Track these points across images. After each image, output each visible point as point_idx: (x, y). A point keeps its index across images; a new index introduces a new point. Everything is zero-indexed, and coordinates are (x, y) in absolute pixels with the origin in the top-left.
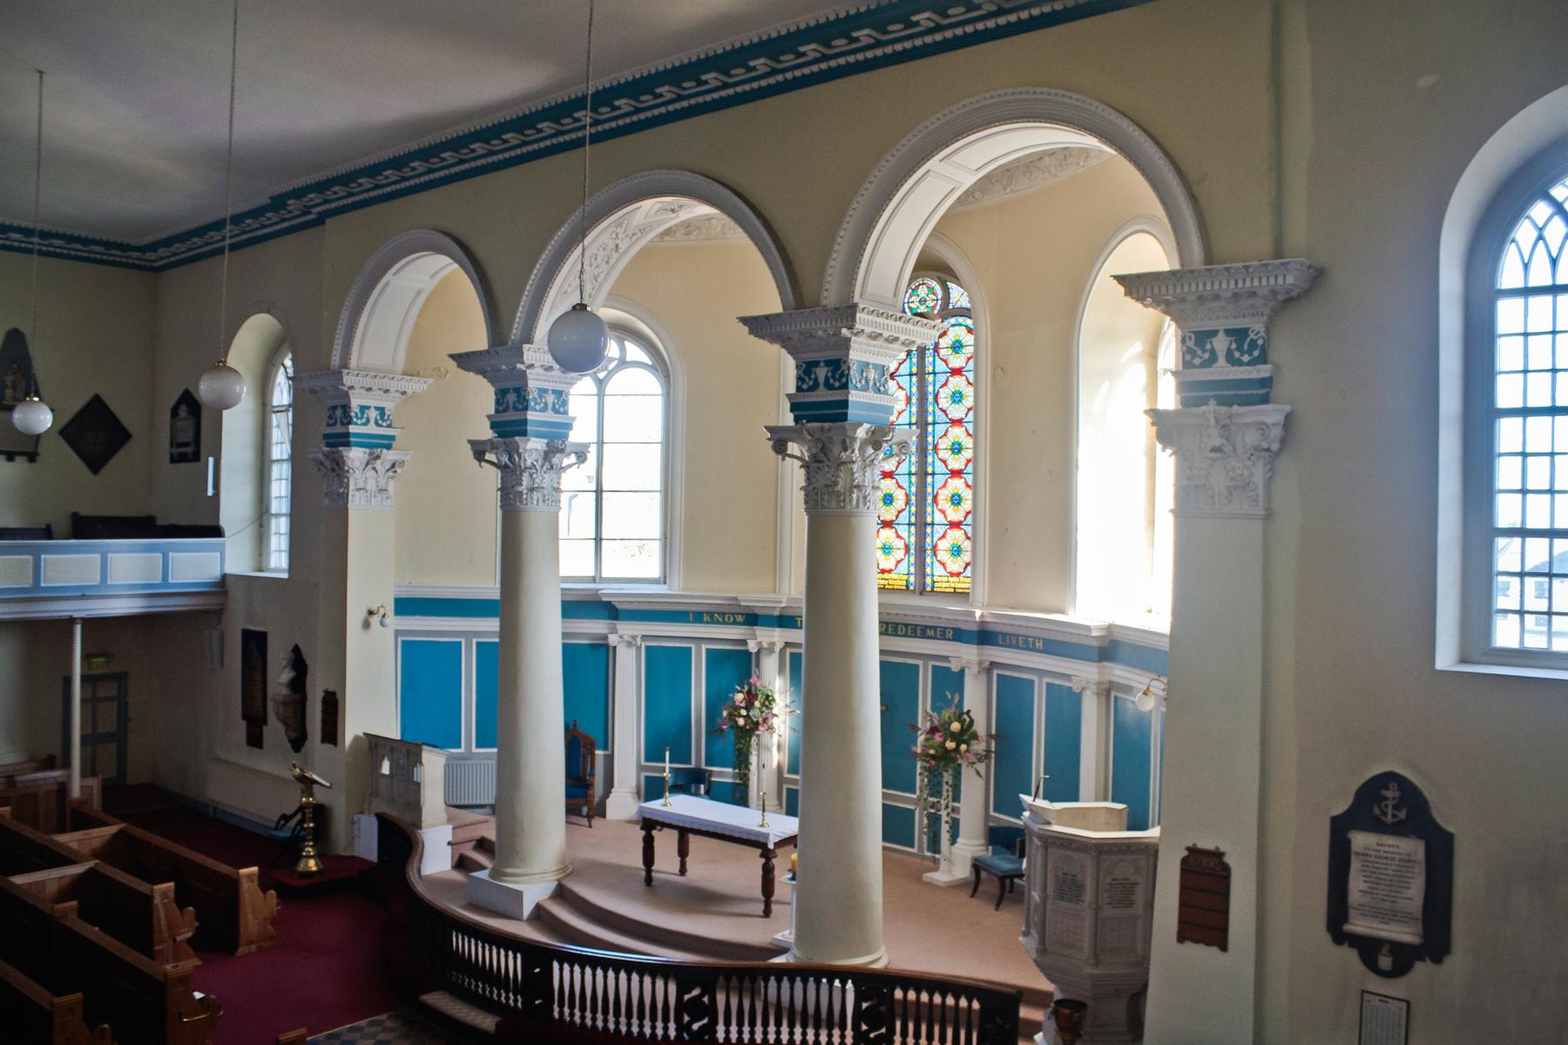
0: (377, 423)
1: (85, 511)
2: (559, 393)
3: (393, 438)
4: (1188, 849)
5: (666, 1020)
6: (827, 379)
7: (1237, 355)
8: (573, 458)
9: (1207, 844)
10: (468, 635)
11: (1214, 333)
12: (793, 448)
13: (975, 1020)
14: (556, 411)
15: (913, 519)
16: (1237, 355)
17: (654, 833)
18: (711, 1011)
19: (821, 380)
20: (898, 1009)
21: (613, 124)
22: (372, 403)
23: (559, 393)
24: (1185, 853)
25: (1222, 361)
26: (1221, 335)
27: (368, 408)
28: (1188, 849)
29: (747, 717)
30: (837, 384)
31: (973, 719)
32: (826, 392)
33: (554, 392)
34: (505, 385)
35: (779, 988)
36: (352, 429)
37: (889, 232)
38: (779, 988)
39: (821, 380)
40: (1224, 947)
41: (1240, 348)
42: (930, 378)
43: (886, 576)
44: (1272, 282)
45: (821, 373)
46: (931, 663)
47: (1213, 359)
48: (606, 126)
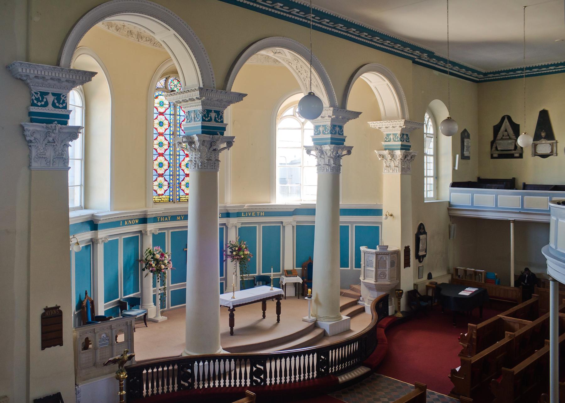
0: (54, 105)
1: (483, 177)
2: (218, 113)
3: (410, 146)
4: (45, 309)
5: (313, 371)
6: (393, 139)
7: (57, 105)
8: (225, 145)
9: (51, 305)
10: (352, 223)
11: (47, 94)
12: (313, 152)
13: (176, 373)
14: (339, 134)
15: (171, 173)
16: (57, 105)
17: (281, 301)
18: (265, 372)
19: (213, 119)
20: (144, 378)
21: (279, 13)
22: (50, 90)
23: (218, 113)
24: (44, 311)
25: (50, 105)
26: (50, 95)
27: (47, 94)
28: (45, 309)
29: (243, 255)
30: (219, 121)
31: (258, 252)
32: (215, 123)
33: (215, 112)
34: (209, 108)
35: (230, 364)
36: (400, 143)
37: (389, 91)
38: (230, 364)
39: (213, 119)
40: (42, 349)
41: (59, 102)
42: (178, 117)
43: (160, 197)
44: (36, 72)
45: (213, 115)
46: (171, 231)
47: (46, 104)
48: (276, 12)
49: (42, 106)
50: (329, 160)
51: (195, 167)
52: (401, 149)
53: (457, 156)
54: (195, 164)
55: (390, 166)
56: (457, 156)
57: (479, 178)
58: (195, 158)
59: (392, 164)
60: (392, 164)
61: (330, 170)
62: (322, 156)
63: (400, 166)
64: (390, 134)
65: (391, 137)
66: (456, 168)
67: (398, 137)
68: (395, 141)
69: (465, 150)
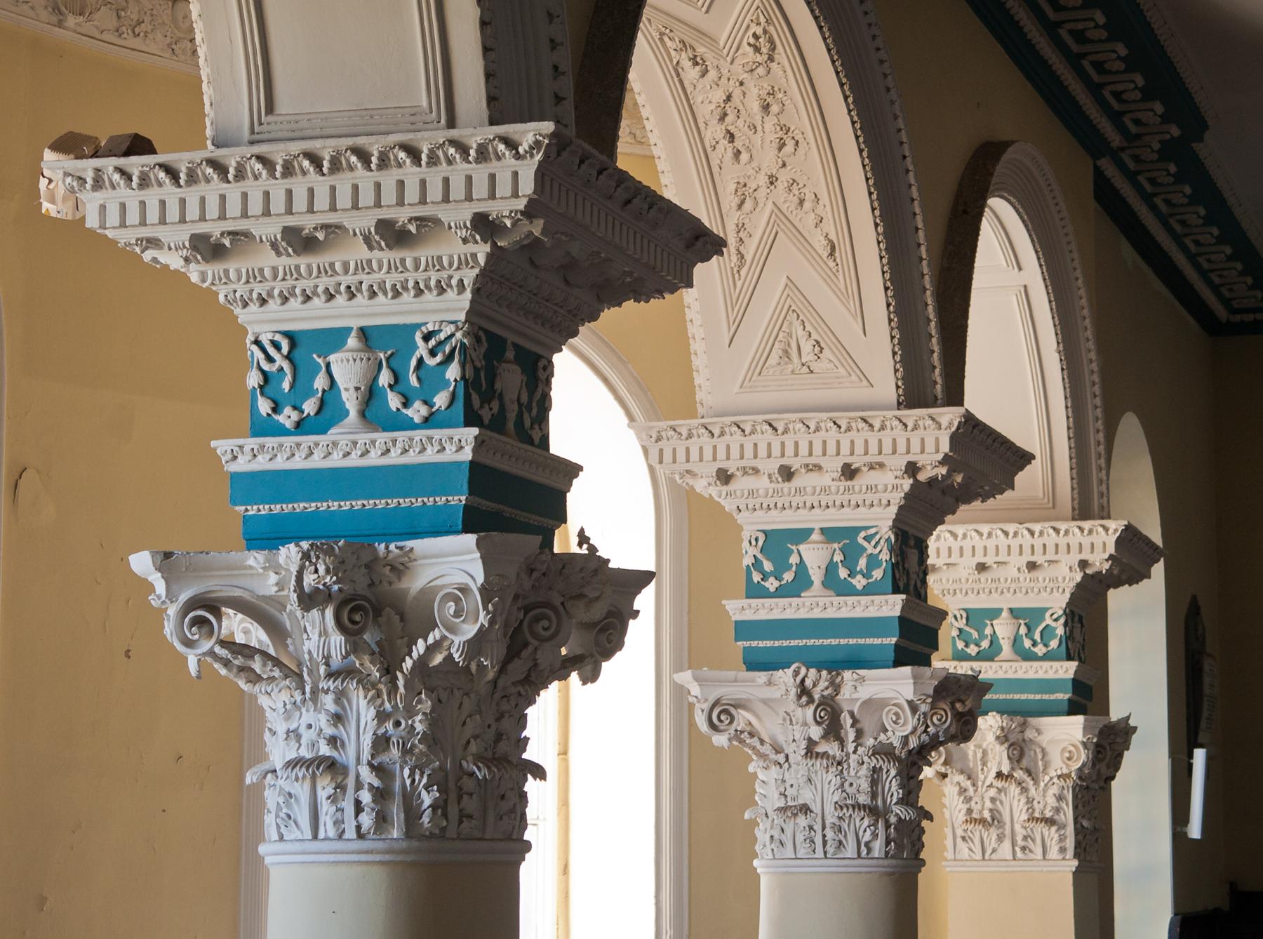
6: (1016, 641)
19: (816, 576)
39: (816, 576)
49: (781, 593)
50: (875, 777)
51: (382, 820)
52: (472, 522)
53: (1199, 756)
54: (381, 795)
55: (997, 819)
56: (1199, 756)
57: (1235, 892)
58: (381, 743)
59: (1014, 806)
60: (1014, 806)
61: (878, 846)
62: (832, 748)
63: (1068, 815)
64: (994, 613)
65: (1003, 629)
66: (1195, 831)
67: (873, 561)
68: (1028, 656)
69: (1203, 725)
